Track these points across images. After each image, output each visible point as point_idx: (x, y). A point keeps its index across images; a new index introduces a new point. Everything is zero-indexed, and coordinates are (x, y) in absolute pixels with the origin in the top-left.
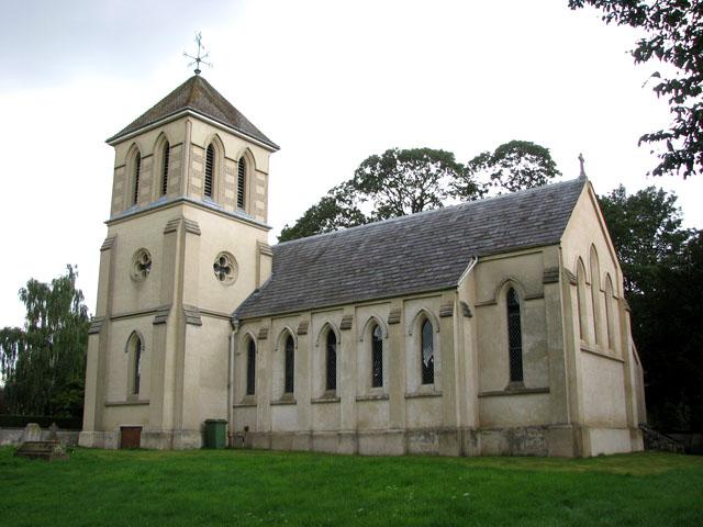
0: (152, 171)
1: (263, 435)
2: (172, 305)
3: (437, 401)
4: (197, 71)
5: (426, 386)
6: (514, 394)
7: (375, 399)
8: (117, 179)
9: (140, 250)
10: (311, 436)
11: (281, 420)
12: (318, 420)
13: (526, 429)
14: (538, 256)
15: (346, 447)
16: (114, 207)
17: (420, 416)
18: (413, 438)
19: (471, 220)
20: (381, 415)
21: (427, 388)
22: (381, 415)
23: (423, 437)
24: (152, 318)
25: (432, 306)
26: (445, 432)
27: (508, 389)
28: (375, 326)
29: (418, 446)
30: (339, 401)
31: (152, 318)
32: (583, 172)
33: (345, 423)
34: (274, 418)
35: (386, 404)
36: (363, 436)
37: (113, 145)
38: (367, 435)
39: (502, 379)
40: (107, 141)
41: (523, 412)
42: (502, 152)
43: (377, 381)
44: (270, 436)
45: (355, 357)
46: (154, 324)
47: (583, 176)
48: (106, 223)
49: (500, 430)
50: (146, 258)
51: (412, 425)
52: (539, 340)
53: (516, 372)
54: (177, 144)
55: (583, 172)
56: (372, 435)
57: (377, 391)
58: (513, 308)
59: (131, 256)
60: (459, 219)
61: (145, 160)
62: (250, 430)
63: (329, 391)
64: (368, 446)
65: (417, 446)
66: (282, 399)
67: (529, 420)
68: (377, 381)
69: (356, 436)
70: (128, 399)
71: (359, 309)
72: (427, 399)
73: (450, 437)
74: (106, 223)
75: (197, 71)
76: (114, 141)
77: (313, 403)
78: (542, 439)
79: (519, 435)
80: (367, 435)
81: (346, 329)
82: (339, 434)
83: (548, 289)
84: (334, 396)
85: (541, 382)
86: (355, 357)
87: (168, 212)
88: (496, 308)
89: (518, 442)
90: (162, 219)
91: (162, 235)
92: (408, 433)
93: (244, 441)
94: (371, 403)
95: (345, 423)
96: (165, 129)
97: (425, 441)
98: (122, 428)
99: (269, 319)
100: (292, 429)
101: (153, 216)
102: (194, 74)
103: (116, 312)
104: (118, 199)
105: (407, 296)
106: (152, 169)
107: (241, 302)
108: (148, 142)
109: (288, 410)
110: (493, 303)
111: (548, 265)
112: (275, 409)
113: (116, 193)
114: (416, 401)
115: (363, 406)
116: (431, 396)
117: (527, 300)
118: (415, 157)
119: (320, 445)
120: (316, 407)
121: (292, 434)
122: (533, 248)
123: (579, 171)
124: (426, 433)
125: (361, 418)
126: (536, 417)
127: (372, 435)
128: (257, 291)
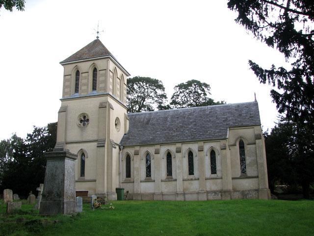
0: (86, 80)
1: (139, 194)
2: (105, 139)
3: (219, 181)
4: (98, 37)
5: (213, 175)
6: (244, 178)
7: (192, 180)
8: (65, 81)
9: (83, 113)
10: (163, 194)
11: (146, 188)
12: (166, 188)
13: (249, 191)
14: (251, 129)
15: (180, 198)
16: (64, 93)
17: (211, 186)
18: (209, 194)
19: (216, 113)
20: (195, 186)
21: (214, 176)
22: (195, 186)
23: (213, 194)
24: (95, 144)
25: (216, 145)
26: (223, 192)
27: (241, 176)
28: (148, 155)
29: (212, 197)
30: (176, 180)
31: (95, 144)
32: (256, 99)
33: (179, 189)
34: (142, 187)
35: (196, 182)
36: (186, 194)
37: (63, 65)
38: (189, 193)
39: (239, 173)
40: (60, 63)
41: (247, 185)
42: (190, 83)
43: (191, 172)
44: (142, 195)
45: (180, 164)
46: (97, 147)
47: (256, 101)
48: (60, 100)
49: (239, 191)
50: (85, 117)
51: (208, 189)
52: (253, 159)
53: (243, 171)
54: (88, 66)
55: (256, 99)
56: (191, 193)
57: (192, 176)
58: (242, 147)
59: (78, 116)
60: (210, 112)
61: (84, 75)
62: (129, 192)
63: (169, 177)
64: (189, 197)
65: (211, 197)
66: (146, 179)
67: (250, 187)
68: (191, 172)
69: (184, 194)
70: (78, 179)
71: (161, 146)
72: (215, 180)
73: (227, 194)
74: (60, 100)
75: (98, 37)
76: (64, 63)
77: (162, 181)
78: (255, 194)
79: (246, 193)
80: (189, 193)
81: (201, 151)
82: (177, 194)
83: (257, 141)
84: (172, 178)
85: (255, 174)
86: (180, 164)
87: (100, 98)
88: (236, 147)
89: (246, 195)
90: (97, 101)
91: (98, 108)
92: (208, 192)
93: (130, 197)
94: (190, 181)
95: (179, 189)
96: (96, 62)
97: (214, 195)
98: (76, 192)
99: (139, 147)
100: (152, 191)
101: (83, 100)
102: (96, 39)
103: (69, 140)
104: (66, 90)
105: (206, 141)
106: (88, 79)
107: (121, 139)
108: (85, 67)
109: (149, 184)
110: (235, 145)
111: (257, 132)
112: (142, 183)
113: (65, 87)
114: (209, 180)
115: (186, 183)
116: (216, 179)
117: (248, 144)
118: (148, 81)
119: (166, 198)
120: (163, 183)
121: (153, 194)
122: (247, 126)
123: (254, 99)
124: (215, 192)
125: (185, 187)
126: (252, 186)
127: (191, 193)
128: (125, 134)
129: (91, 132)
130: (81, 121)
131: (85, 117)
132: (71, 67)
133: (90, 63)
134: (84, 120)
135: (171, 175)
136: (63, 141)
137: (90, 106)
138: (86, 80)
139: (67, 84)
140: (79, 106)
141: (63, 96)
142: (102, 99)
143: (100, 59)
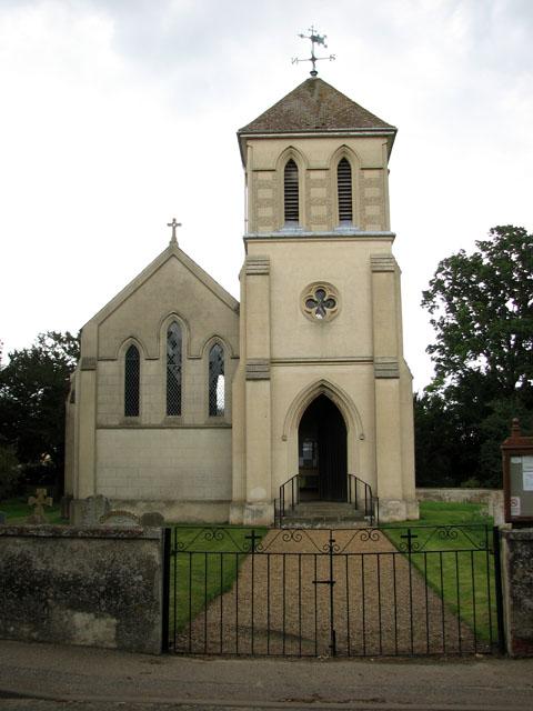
0: (318, 192)
4: (314, 73)
50: (321, 292)
75: (314, 73)
90: (364, 251)
102: (310, 76)
103: (280, 354)
108: (318, 153)
129: (349, 332)
130: (310, 302)
131: (321, 292)
132: (270, 152)
133: (335, 144)
134: (321, 300)
135: (179, 413)
136: (95, 356)
137: (341, 264)
138: (318, 192)
139: (372, 210)
140: (299, 264)
141: (253, 228)
142: (376, 248)
143: (369, 136)
